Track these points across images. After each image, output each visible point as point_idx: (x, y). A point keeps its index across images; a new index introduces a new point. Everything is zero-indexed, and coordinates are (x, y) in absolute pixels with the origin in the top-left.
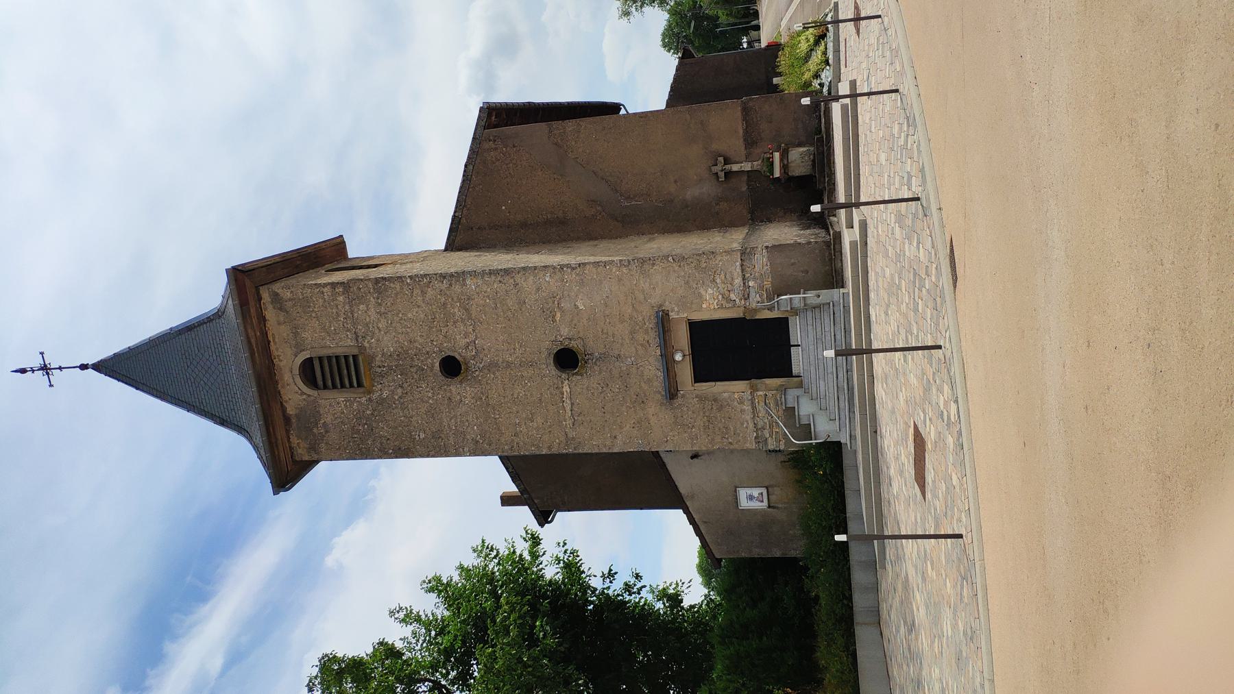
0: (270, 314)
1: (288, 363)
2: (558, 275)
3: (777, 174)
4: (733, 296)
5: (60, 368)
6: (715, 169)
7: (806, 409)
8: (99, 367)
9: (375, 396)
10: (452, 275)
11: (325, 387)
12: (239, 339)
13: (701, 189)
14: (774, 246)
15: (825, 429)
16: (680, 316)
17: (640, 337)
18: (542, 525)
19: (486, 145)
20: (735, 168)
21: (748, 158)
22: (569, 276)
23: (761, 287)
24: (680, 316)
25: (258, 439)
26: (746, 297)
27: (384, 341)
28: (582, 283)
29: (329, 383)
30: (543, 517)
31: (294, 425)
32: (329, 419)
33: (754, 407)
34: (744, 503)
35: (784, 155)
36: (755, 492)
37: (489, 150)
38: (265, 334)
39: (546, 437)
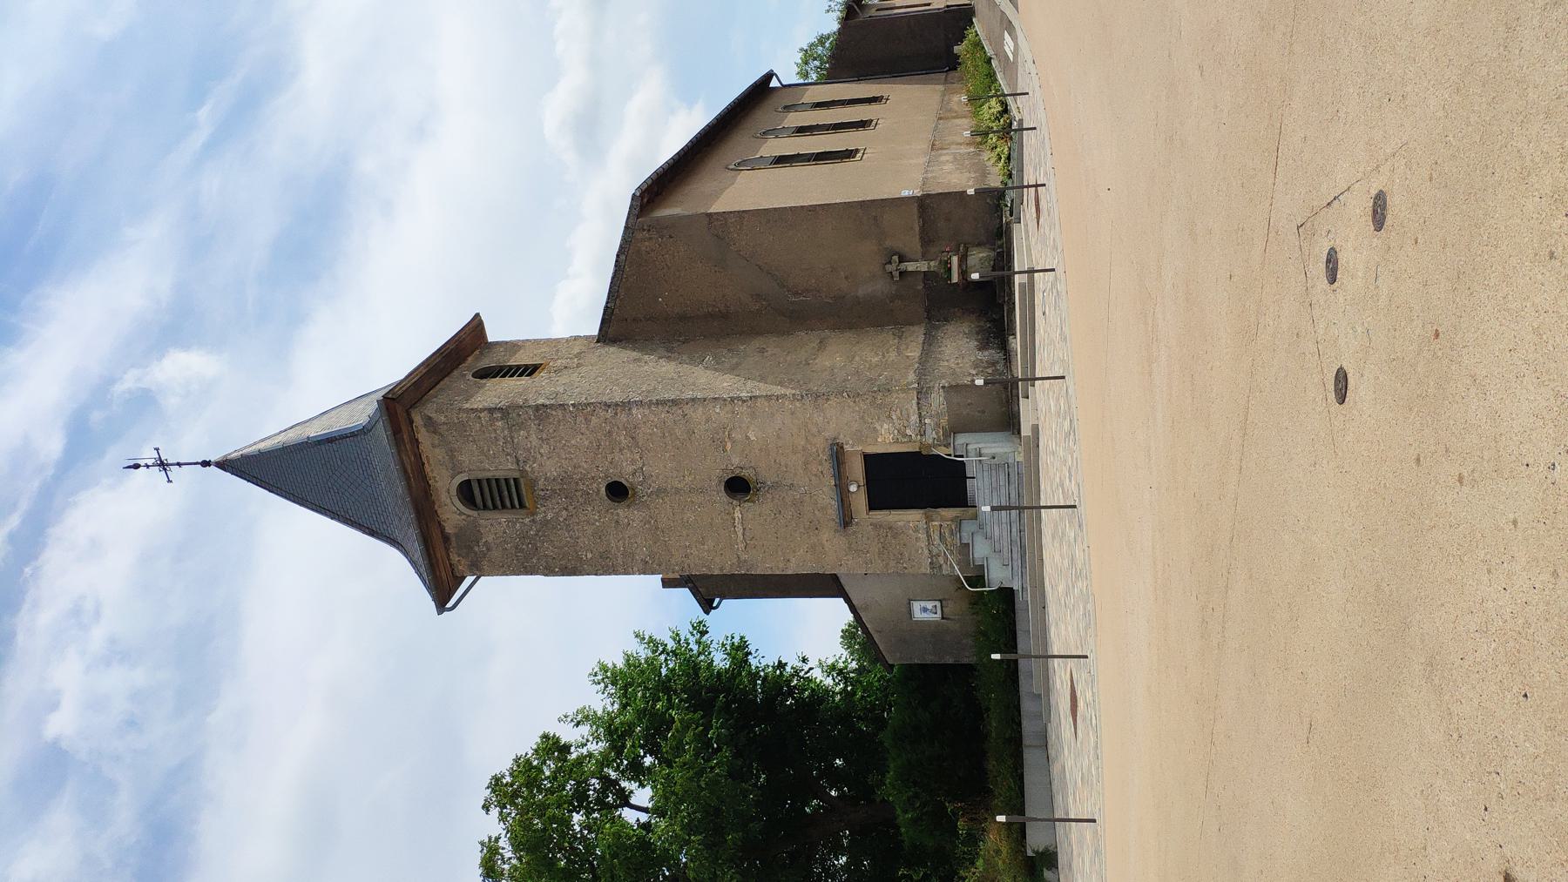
0: (423, 436)
1: (445, 486)
2: (729, 407)
3: (955, 279)
4: (908, 432)
5: (179, 464)
6: (889, 268)
7: (980, 550)
8: (224, 465)
9: (538, 518)
10: (617, 405)
11: (485, 507)
12: (394, 468)
13: (874, 286)
14: (951, 387)
15: (998, 576)
16: (855, 449)
17: (814, 468)
18: (707, 612)
19: (639, 235)
20: (911, 266)
21: (925, 257)
22: (741, 409)
23: (938, 425)
24: (855, 449)
25: (418, 555)
26: (923, 434)
27: (546, 466)
28: (753, 415)
29: (489, 503)
30: (707, 606)
31: (454, 544)
32: (490, 538)
33: (929, 536)
34: (918, 615)
35: (963, 259)
36: (929, 605)
37: (643, 240)
38: (418, 456)
39: (717, 560)
